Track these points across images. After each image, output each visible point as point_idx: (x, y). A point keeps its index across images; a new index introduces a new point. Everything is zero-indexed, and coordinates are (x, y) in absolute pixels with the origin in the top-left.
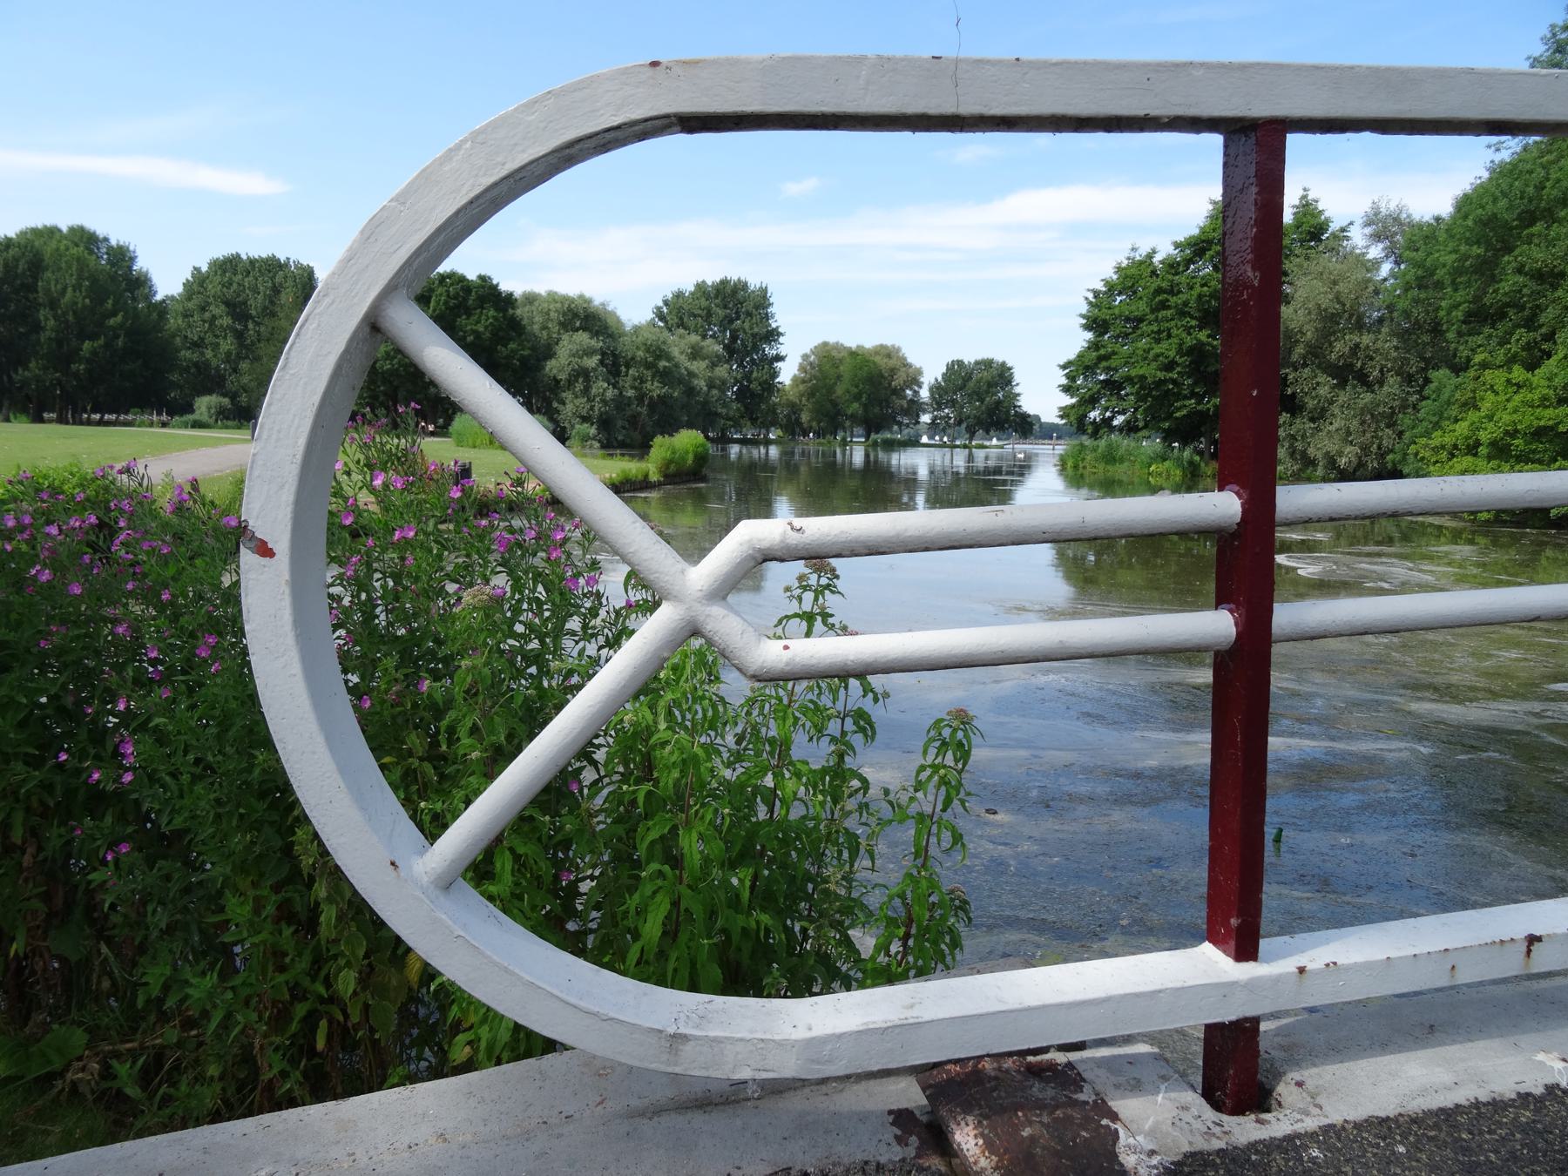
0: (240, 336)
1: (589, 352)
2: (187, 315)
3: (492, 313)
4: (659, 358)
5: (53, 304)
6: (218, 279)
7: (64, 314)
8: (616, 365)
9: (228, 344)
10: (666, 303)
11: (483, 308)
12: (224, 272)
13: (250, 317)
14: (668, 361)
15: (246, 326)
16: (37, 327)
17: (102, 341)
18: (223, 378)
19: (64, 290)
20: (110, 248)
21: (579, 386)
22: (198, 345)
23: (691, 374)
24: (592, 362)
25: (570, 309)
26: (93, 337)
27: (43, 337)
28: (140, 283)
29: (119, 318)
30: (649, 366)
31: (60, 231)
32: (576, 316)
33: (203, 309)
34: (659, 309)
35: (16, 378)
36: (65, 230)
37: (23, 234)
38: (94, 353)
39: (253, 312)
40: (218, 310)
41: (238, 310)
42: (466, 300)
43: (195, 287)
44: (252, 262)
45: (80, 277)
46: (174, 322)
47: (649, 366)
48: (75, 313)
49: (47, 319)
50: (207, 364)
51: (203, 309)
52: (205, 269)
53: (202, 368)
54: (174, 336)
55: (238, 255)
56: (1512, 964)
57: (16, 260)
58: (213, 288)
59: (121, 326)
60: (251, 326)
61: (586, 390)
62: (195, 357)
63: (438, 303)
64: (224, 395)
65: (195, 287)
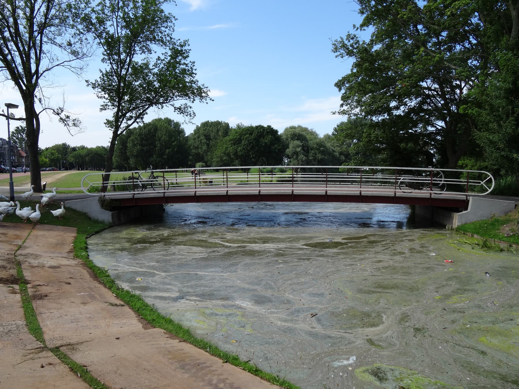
0: (208, 145)
1: (298, 146)
2: (194, 139)
3: (270, 136)
4: (321, 147)
5: (159, 140)
6: (202, 129)
7: (162, 142)
8: (308, 150)
9: (205, 148)
10: (338, 126)
11: (268, 135)
12: (205, 126)
13: (211, 139)
14: (324, 148)
15: (210, 142)
16: (155, 146)
17: (171, 149)
18: (203, 157)
19: (163, 135)
20: (174, 123)
21: (295, 157)
22: (197, 148)
23: (334, 151)
24: (299, 149)
25: (294, 134)
26: (169, 148)
27: (157, 149)
28: (182, 132)
29: (175, 143)
30: (318, 149)
31: (162, 119)
32: (296, 135)
33: (199, 137)
34: (335, 128)
35: (150, 160)
36: (163, 119)
37: (153, 121)
38: (169, 152)
39: (212, 138)
40: (202, 137)
41: (208, 137)
42: (263, 133)
43: (197, 131)
44: (212, 123)
45: (166, 132)
46: (190, 143)
47: (318, 149)
48: (165, 142)
49: (158, 144)
50: (199, 153)
51: (199, 137)
52: (199, 126)
53: (198, 155)
54: (190, 147)
55: (208, 121)
56: (162, 195)
57: (151, 128)
58: (201, 131)
59: (176, 145)
60: (211, 142)
61: (297, 158)
62: (196, 152)
63: (254, 135)
64: (204, 162)
65: (197, 131)
